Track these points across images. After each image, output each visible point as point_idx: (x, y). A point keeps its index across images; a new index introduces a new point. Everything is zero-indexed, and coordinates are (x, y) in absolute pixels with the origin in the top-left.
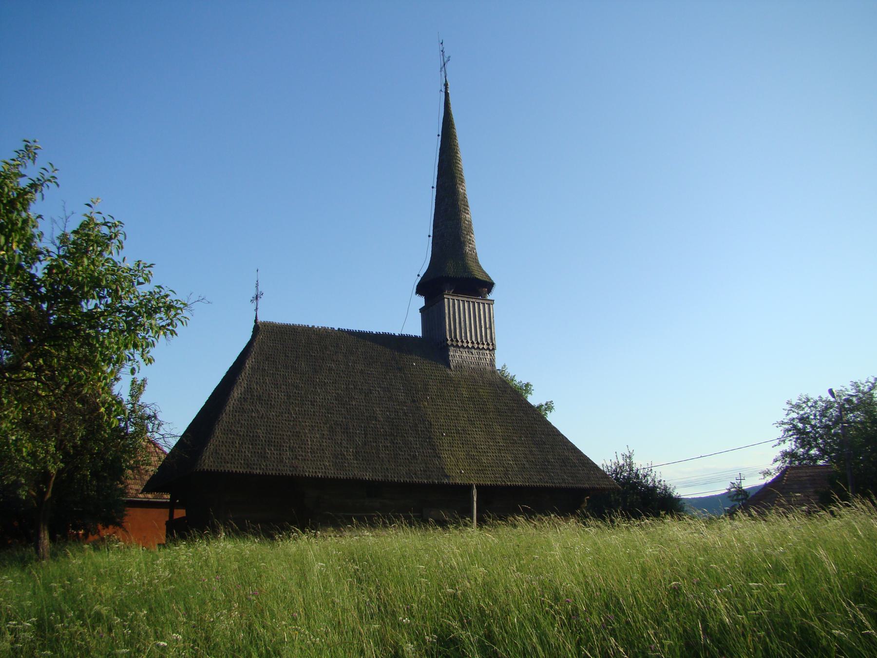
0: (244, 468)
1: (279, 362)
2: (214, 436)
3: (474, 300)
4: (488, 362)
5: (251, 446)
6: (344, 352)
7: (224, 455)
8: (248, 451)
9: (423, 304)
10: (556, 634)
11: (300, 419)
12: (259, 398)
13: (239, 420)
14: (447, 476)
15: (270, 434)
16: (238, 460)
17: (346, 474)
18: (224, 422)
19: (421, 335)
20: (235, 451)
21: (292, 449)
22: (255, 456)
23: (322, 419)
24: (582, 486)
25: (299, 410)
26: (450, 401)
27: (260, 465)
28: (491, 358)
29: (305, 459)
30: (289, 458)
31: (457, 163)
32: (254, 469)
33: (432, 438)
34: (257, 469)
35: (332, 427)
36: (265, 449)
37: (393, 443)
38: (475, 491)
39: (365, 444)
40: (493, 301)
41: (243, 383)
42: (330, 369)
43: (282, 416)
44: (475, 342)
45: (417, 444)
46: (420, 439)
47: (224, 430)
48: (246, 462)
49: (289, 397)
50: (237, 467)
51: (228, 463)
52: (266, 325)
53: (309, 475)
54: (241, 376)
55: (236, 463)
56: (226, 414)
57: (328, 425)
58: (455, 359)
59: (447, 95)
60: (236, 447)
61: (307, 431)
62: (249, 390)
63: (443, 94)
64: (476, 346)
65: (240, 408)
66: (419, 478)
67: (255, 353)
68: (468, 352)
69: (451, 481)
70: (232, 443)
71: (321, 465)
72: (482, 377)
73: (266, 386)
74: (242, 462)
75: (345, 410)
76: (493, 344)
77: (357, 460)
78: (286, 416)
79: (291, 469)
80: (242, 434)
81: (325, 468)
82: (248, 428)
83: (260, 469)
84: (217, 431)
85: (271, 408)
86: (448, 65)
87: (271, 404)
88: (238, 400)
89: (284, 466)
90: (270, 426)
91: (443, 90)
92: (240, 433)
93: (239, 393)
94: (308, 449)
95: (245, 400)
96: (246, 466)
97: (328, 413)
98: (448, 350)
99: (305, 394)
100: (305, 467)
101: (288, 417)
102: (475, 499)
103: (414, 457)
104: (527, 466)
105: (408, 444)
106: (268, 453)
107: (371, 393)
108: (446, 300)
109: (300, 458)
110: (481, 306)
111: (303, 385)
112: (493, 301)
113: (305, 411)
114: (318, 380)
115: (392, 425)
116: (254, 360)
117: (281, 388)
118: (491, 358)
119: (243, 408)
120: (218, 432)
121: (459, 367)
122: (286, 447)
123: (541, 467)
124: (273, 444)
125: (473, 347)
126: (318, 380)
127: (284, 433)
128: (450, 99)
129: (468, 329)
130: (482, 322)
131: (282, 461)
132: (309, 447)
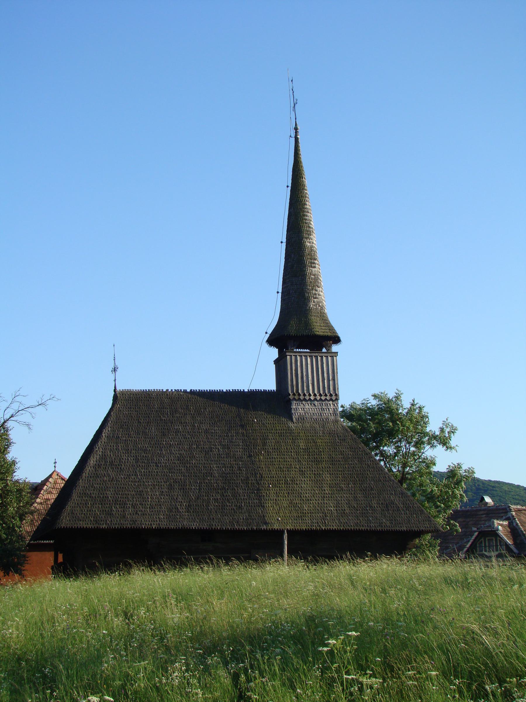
0: (93, 524)
1: (132, 429)
2: (71, 499)
3: (317, 354)
4: (331, 412)
5: (100, 506)
6: (193, 413)
7: (78, 514)
8: (98, 510)
9: (278, 357)
10: (87, 570)
11: (144, 480)
12: (111, 463)
13: (93, 483)
14: (266, 523)
15: (117, 494)
16: (89, 517)
17: (176, 525)
18: (81, 487)
19: (275, 389)
20: (87, 510)
21: (133, 506)
22: (103, 514)
23: (163, 479)
24: (398, 529)
25: (144, 472)
26: (286, 453)
27: (106, 521)
28: (334, 407)
29: (144, 514)
30: (131, 514)
31: (304, 215)
32: (101, 524)
33: (261, 490)
34: (103, 524)
35: (171, 485)
36: (111, 507)
37: (224, 495)
38: (286, 536)
39: (198, 498)
40: (337, 353)
41: (98, 451)
42: (177, 431)
43: (129, 478)
44: (318, 395)
45: (245, 495)
46: (249, 491)
47: (80, 493)
48: (95, 519)
49: (137, 460)
50: (88, 524)
51: (81, 520)
52: (123, 393)
53: (145, 527)
54: (98, 445)
55: (87, 520)
56: (82, 480)
57: (168, 483)
58: (298, 411)
59: (297, 140)
60: (88, 507)
61: (149, 490)
62: (104, 457)
63: (293, 140)
64: (318, 398)
65: (94, 473)
66: (239, 525)
67: (112, 422)
68: (311, 404)
69: (269, 527)
70: (86, 504)
71: (156, 518)
72: (323, 427)
73: (118, 453)
74: (92, 519)
75: (186, 468)
76: (336, 395)
77: (188, 512)
78: (133, 477)
79: (131, 523)
80: (94, 496)
81: (159, 520)
82: (99, 490)
83: (106, 524)
84: (74, 495)
85: (120, 472)
86: (297, 106)
87: (121, 468)
88: (93, 467)
89: (125, 521)
90: (118, 488)
91: (293, 135)
92: (93, 495)
93: (95, 460)
94: (148, 505)
95: (99, 466)
96: (94, 523)
97: (170, 473)
98: (290, 404)
99: (151, 456)
100: (143, 521)
101: (134, 478)
102: (286, 542)
103: (240, 507)
104: (347, 511)
105: (237, 496)
106: (114, 510)
107: (211, 451)
108: (288, 357)
109: (140, 513)
110: (324, 359)
111: (150, 449)
112: (337, 353)
113: (149, 472)
114: (164, 443)
115: (226, 480)
116: (110, 429)
117: (131, 452)
118: (334, 407)
119: (97, 474)
120: (75, 496)
121: (302, 419)
122: (130, 504)
123: (361, 512)
124: (118, 503)
125: (315, 399)
126: (164, 443)
127: (129, 493)
128: (300, 145)
129: (310, 382)
130: (325, 375)
131: (124, 517)
132: (149, 503)
